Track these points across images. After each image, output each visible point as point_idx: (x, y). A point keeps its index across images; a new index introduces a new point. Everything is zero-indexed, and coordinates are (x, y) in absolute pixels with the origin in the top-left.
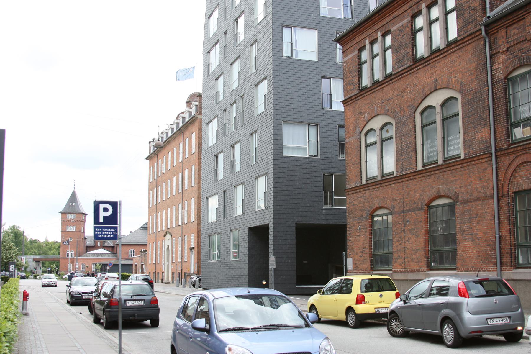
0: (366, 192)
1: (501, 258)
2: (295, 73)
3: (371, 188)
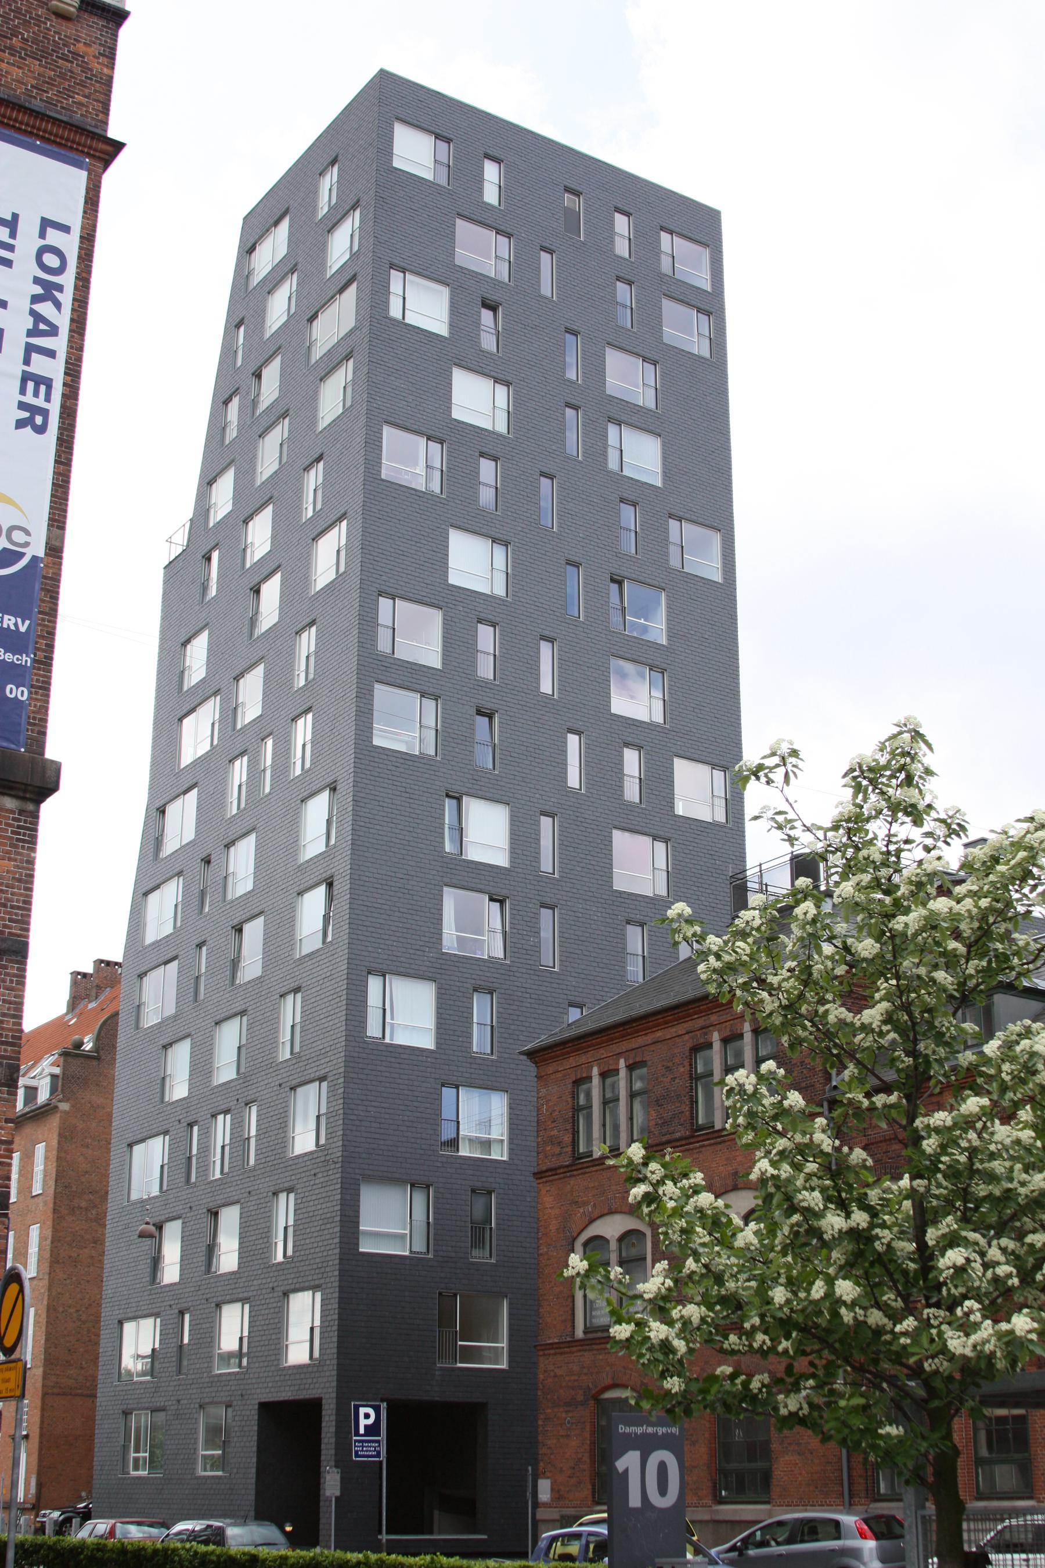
0: (586, 1354)
1: (850, 1484)
2: (388, 1075)
3: (595, 1347)
